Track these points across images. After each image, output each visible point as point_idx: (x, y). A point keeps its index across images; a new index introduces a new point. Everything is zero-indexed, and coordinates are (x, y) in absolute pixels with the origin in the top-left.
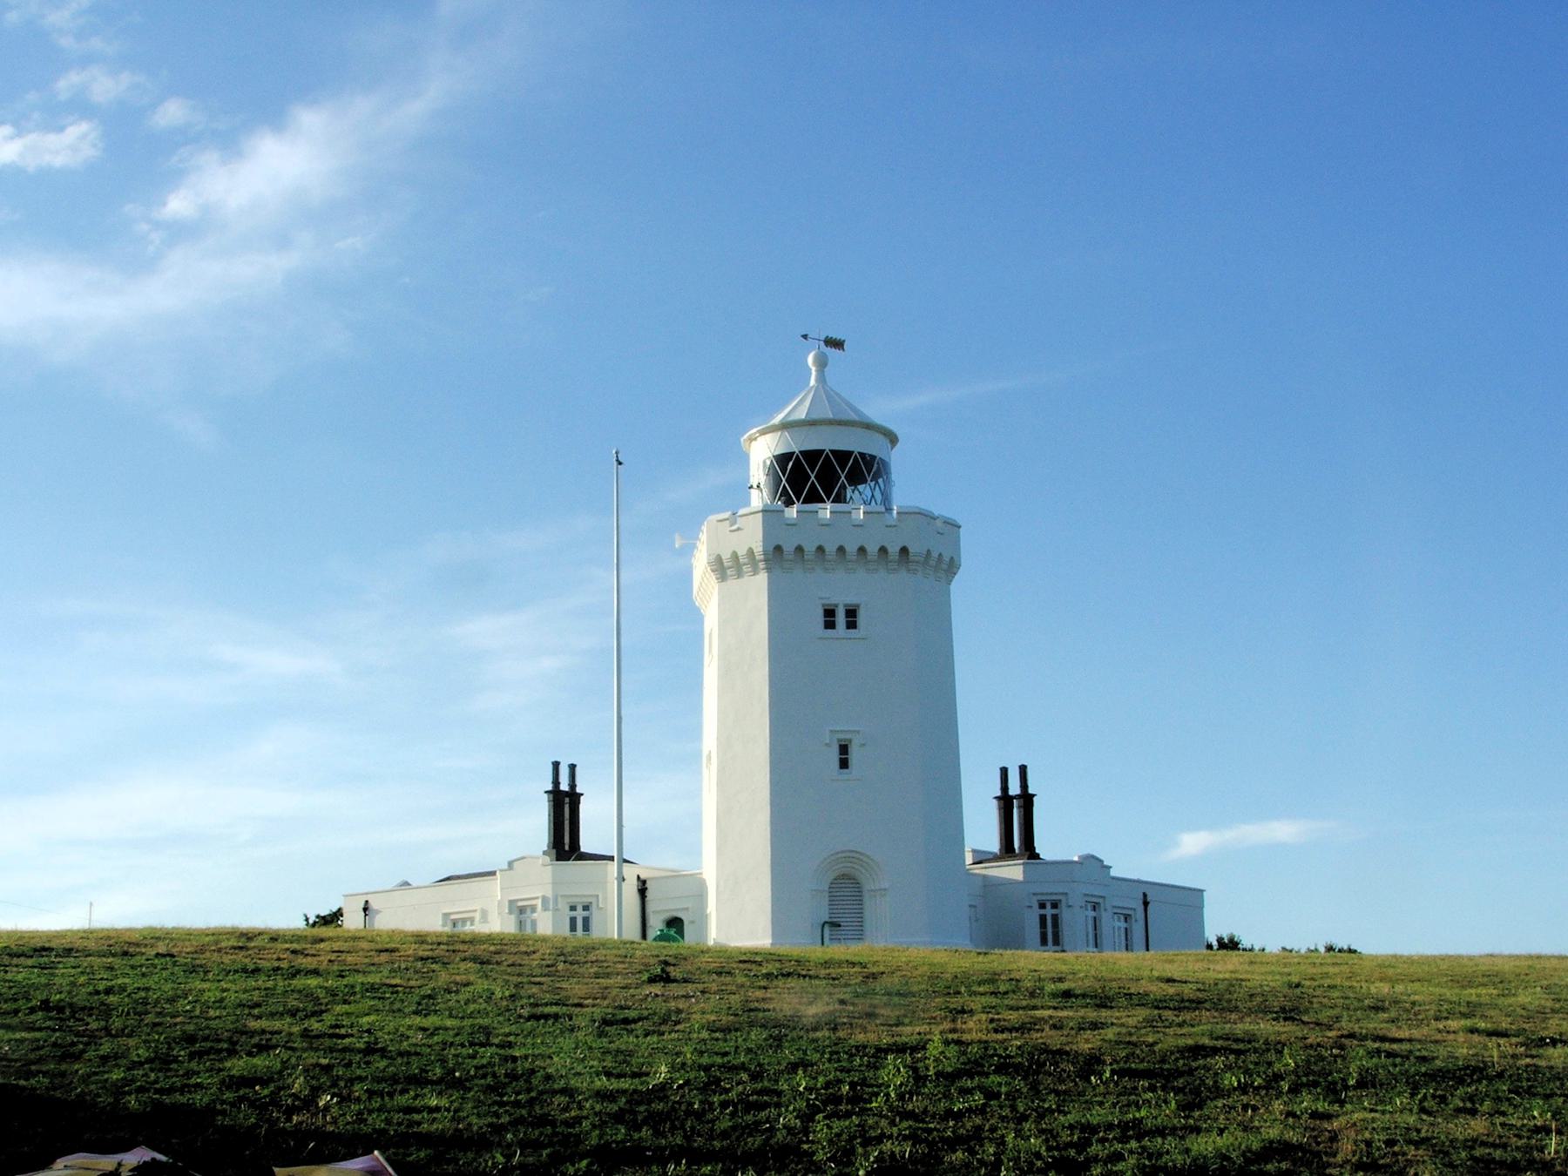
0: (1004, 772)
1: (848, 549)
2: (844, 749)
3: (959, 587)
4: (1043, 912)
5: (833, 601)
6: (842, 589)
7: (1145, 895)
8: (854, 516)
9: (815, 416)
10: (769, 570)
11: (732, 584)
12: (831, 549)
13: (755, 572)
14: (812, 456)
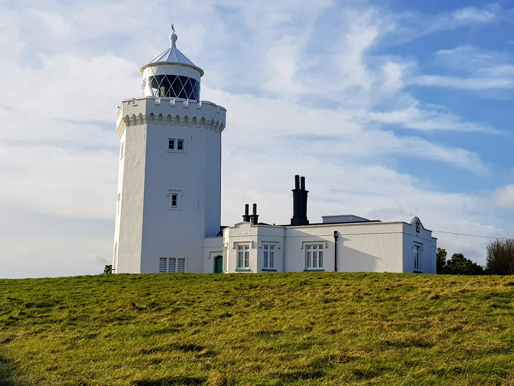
0: (247, 206)
2: (174, 197)
3: (224, 134)
4: (266, 250)
6: (177, 133)
7: (300, 181)
8: (184, 103)
12: (174, 116)
13: (142, 123)
14: (171, 77)
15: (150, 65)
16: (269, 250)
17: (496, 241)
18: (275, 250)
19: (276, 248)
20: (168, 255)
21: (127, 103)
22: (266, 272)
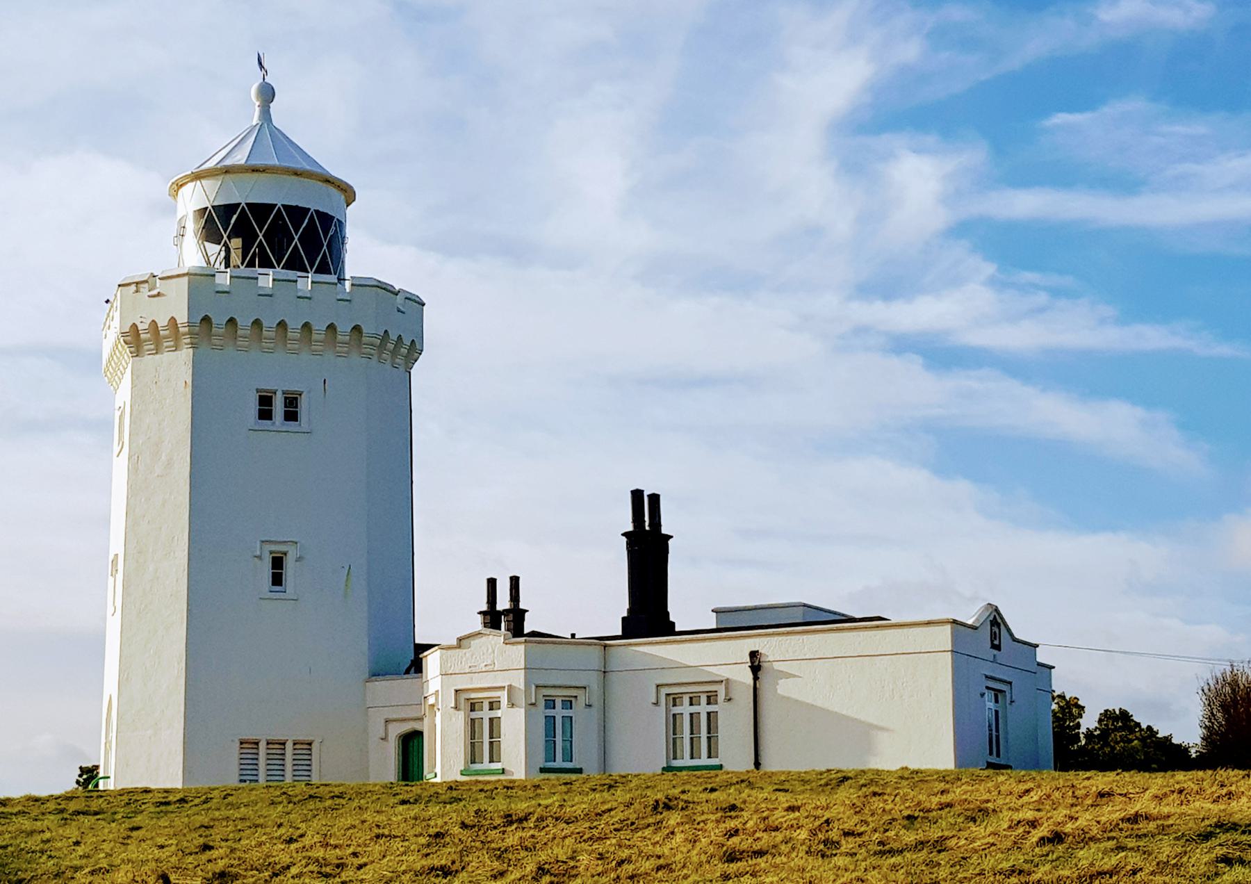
0: (492, 583)
1: (265, 324)
2: (278, 563)
4: (550, 712)
5: (267, 386)
6: (280, 372)
7: (645, 507)
8: (261, 283)
9: (255, 162)
10: (194, 346)
11: (148, 360)
13: (176, 348)
19: (579, 705)
20: (262, 734)
21: (133, 288)
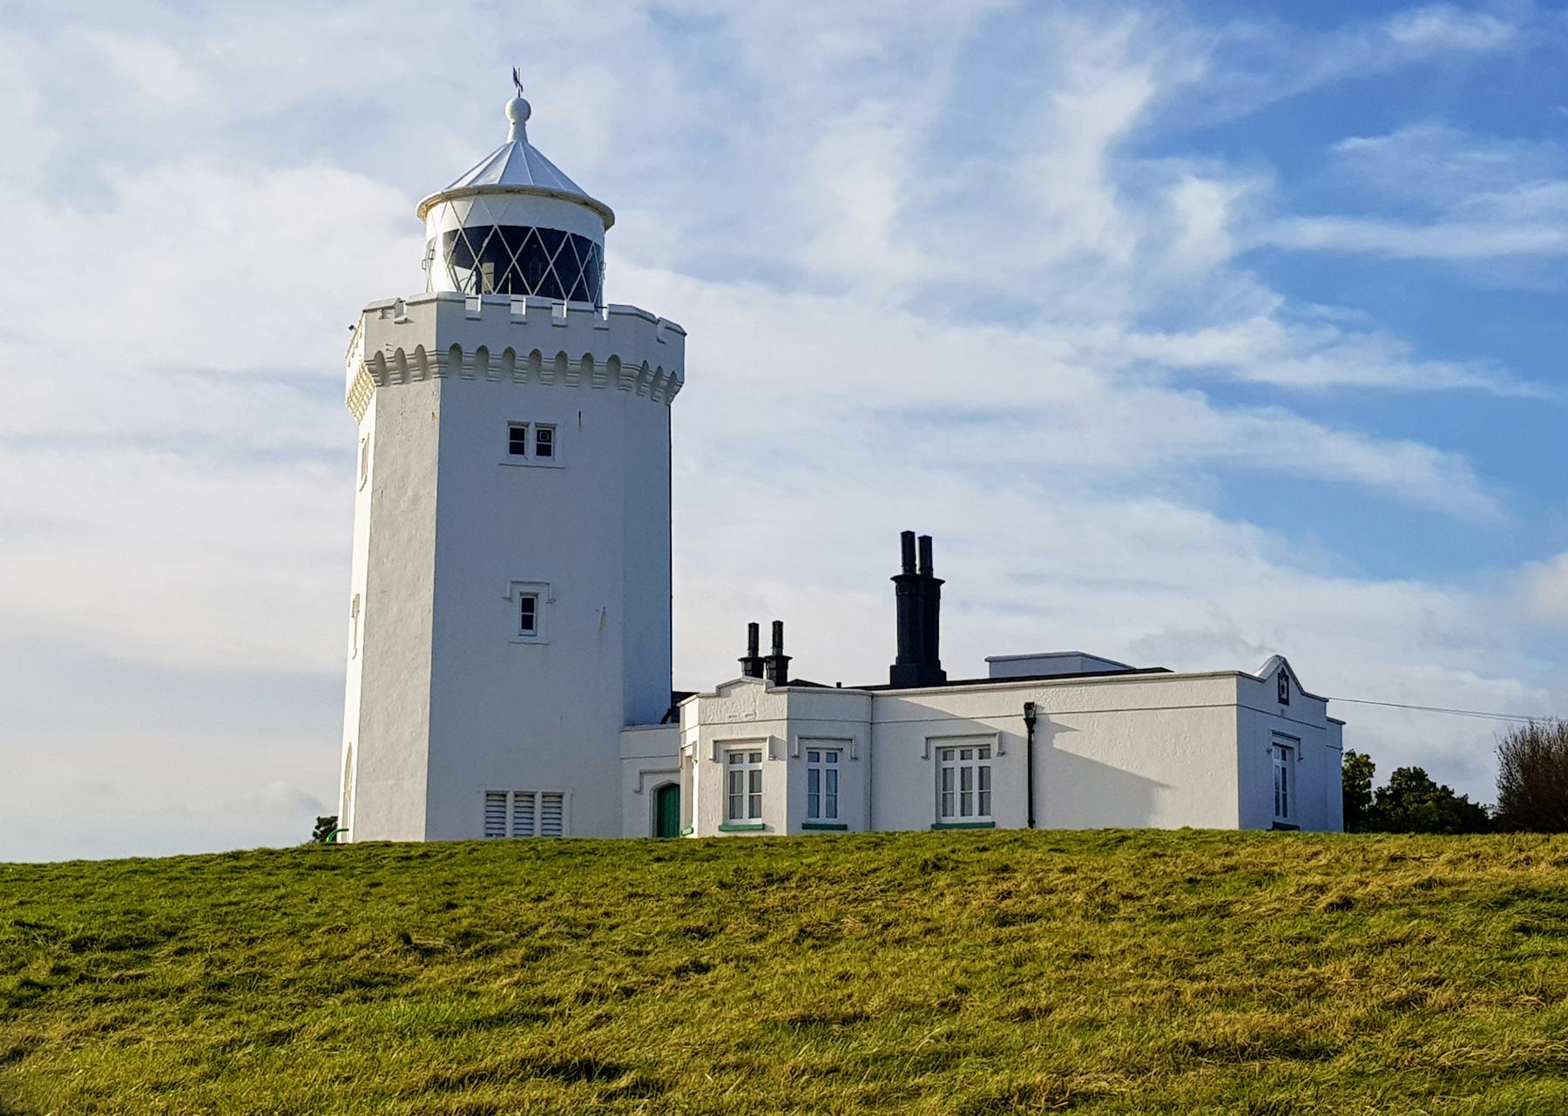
0: (754, 628)
1: (518, 353)
2: (528, 604)
3: (680, 406)
4: (814, 766)
6: (532, 404)
7: (916, 548)
8: (555, 313)
9: (511, 182)
10: (443, 375)
11: (394, 389)
13: (424, 377)
14: (514, 234)
15: (448, 197)
16: (823, 766)
17: (1528, 726)
18: (843, 765)
19: (844, 758)
22: (816, 833)
